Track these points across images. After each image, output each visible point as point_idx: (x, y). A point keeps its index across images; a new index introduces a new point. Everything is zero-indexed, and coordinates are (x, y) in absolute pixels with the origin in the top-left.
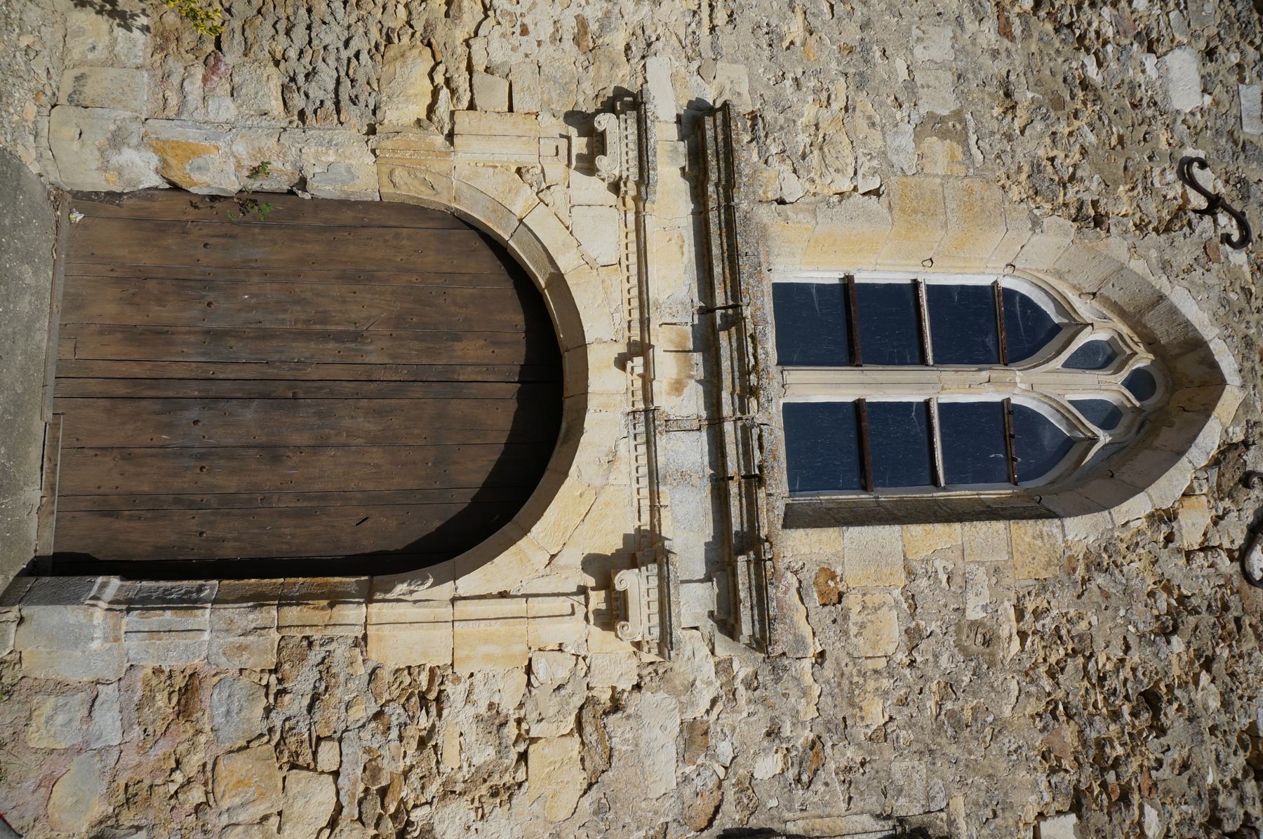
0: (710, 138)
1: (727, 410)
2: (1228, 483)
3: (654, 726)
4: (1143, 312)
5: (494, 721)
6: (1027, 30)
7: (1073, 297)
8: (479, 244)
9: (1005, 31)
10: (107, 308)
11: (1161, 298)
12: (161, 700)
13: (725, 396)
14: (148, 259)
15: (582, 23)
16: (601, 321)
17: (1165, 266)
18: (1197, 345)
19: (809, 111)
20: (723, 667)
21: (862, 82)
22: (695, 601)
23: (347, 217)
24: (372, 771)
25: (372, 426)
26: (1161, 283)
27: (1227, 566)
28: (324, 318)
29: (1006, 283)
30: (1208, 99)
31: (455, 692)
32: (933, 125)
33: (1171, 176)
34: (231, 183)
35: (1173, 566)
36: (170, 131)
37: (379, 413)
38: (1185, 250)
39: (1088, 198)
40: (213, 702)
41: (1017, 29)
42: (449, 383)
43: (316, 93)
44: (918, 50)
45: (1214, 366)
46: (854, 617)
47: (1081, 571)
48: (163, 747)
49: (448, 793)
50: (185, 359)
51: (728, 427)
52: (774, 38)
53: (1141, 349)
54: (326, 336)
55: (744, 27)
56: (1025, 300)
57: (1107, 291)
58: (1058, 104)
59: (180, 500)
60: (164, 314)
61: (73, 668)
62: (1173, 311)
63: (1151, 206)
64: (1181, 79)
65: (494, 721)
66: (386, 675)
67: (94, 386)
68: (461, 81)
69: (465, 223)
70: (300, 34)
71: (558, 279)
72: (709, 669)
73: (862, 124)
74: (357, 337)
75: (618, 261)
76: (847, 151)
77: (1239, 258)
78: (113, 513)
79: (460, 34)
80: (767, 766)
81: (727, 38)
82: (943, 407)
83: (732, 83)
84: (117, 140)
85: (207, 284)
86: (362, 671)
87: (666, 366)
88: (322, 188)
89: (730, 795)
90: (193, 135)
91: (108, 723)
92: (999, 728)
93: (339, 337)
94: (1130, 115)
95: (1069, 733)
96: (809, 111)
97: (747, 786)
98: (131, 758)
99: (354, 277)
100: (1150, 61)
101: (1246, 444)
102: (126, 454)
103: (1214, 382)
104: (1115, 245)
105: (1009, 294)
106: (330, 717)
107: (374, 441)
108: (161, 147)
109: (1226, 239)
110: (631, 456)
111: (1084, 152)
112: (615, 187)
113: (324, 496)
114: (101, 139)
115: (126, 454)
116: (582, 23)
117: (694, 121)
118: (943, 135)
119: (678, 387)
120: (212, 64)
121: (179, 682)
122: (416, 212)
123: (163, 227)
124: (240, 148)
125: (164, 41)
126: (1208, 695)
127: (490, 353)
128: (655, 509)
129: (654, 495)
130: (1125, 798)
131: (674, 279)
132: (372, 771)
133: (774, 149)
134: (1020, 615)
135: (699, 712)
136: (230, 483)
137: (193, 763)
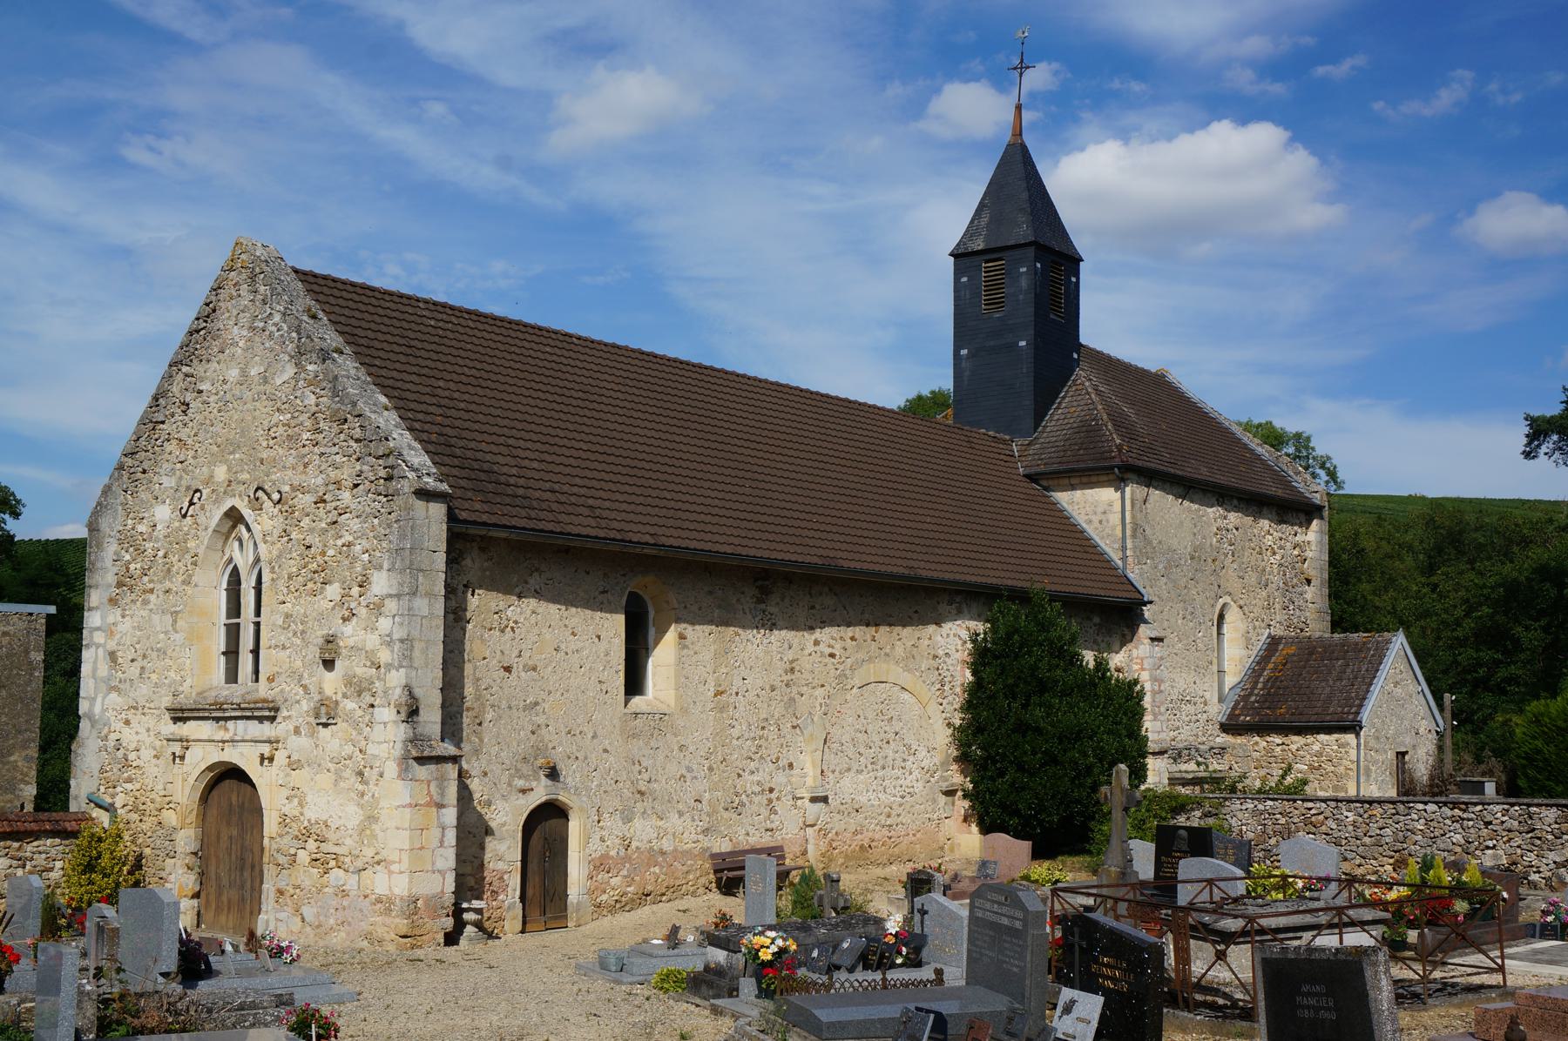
0: (180, 715)
9: (152, 591)
10: (223, 918)
16: (216, 756)
19: (172, 674)
29: (225, 585)
35: (276, 533)
38: (202, 519)
58: (169, 570)
64: (163, 513)
69: (205, 798)
71: (210, 768)
75: (208, 746)
87: (221, 735)
88: (193, 847)
91: (282, 915)
99: (218, 838)
100: (159, 527)
104: (201, 551)
117: (176, 720)
119: (227, 729)
122: (203, 817)
123: (207, 901)
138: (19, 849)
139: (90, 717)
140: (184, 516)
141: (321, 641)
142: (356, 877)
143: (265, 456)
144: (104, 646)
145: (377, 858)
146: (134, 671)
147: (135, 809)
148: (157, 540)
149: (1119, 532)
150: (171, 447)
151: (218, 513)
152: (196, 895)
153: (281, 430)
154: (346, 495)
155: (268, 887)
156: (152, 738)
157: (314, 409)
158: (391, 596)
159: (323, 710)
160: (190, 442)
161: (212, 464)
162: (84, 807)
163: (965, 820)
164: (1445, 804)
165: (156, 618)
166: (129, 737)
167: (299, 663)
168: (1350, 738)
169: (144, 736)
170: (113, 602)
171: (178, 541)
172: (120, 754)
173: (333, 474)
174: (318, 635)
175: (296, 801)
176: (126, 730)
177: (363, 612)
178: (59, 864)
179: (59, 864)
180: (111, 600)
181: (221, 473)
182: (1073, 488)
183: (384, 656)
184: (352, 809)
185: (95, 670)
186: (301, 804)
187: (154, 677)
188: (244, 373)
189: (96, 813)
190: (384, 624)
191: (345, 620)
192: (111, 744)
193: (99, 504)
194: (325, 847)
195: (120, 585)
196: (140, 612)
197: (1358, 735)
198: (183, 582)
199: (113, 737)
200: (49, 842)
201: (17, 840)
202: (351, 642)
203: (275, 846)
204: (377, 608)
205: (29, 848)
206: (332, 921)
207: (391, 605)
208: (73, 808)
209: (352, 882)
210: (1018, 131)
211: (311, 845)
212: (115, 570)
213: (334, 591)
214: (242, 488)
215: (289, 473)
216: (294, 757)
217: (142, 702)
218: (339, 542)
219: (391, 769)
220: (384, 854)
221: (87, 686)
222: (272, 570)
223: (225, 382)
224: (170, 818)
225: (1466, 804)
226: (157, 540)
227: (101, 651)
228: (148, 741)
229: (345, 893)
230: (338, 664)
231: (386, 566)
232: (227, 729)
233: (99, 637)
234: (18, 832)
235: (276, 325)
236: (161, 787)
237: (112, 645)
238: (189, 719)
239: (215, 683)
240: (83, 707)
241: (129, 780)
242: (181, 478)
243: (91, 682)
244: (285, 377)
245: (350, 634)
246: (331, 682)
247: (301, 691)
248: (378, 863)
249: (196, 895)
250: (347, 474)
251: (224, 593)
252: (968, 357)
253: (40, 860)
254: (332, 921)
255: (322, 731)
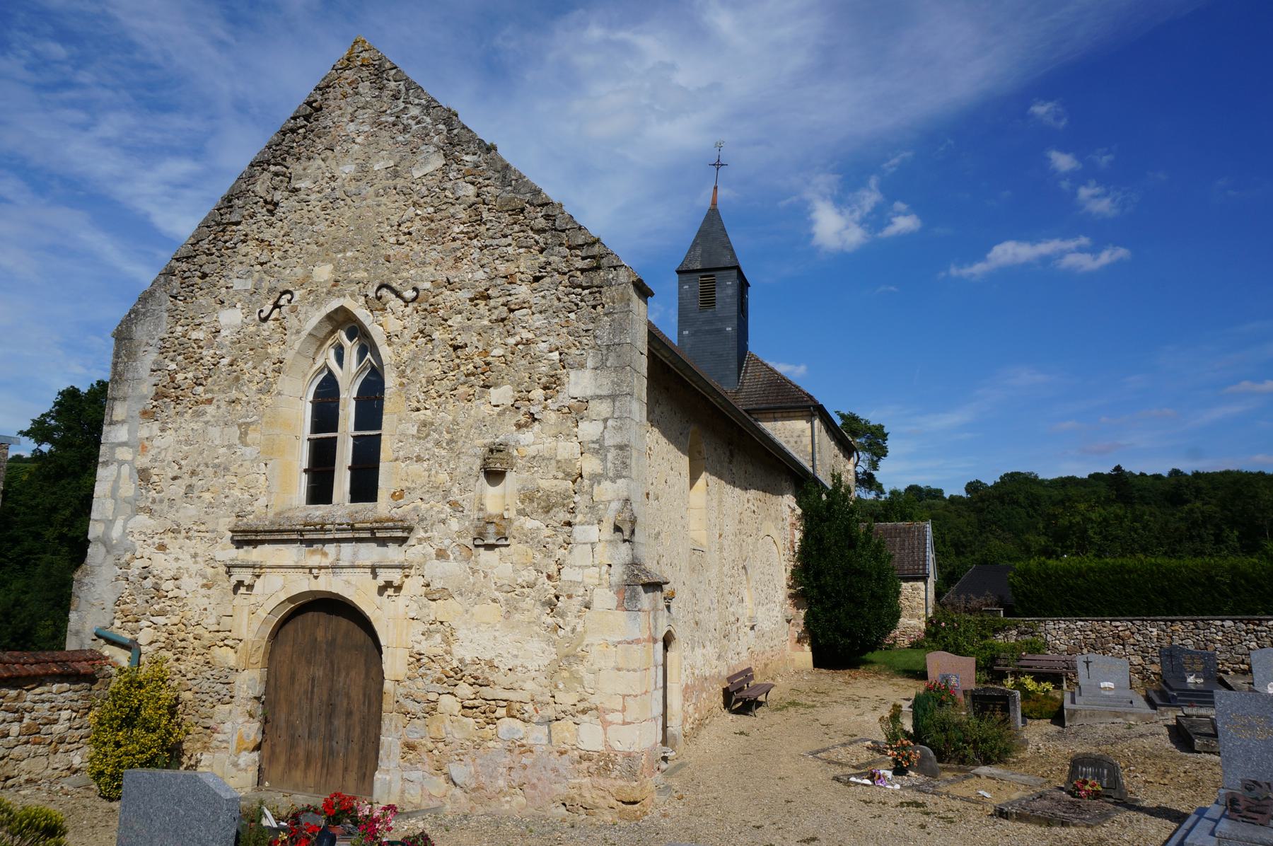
0: (246, 538)
1: (331, 536)
2: (380, 306)
3: (439, 571)
4: (318, 340)
5: (427, 634)
6: (212, 391)
7: (316, 367)
8: (283, 630)
9: (210, 401)
10: (298, 775)
11: (310, 334)
12: (410, 756)
13: (327, 537)
14: (283, 759)
15: (204, 586)
16: (303, 584)
17: (298, 332)
18: (329, 317)
19: (236, 492)
20: (420, 541)
21: (226, 469)
22: (393, 553)
23: (272, 682)
24: (439, 680)
25: (343, 674)
26: (304, 334)
27: (409, 310)
28: (306, 692)
29: (311, 397)
30: (239, 305)
31: (417, 648)
32: (243, 435)
33: (265, 325)
34: (256, 725)
35: (407, 335)
36: (233, 746)
37: (339, 671)
38: (292, 322)
39: (272, 367)
40: (413, 738)
41: (209, 396)
42: (332, 643)
43: (224, 692)
44: (216, 442)
45: (337, 310)
46: (408, 484)
47: (405, 380)
48: (424, 756)
49: (449, 653)
50: (317, 746)
51: (337, 536)
52: (210, 505)
53: (337, 335)
54: (312, 692)
55: (206, 518)
56: (318, 387)
57: (311, 354)
58: (237, 379)
59: (361, 750)
60: (301, 753)
61: (397, 787)
62: (315, 328)
63: (277, 336)
64: (231, 318)
65: (427, 634)
66: (409, 673)
67: (323, 781)
68: (222, 635)
69: (275, 635)
70: (204, 697)
71: (291, 600)
72: (419, 547)
73: (242, 469)
74: (313, 680)
75: (286, 575)
76: (250, 477)
77: (297, 295)
78: (365, 775)
79: (207, 635)
80: (454, 525)
81: (210, 526)
82: (357, 428)
83: (225, 524)
84: (235, 765)
85: (293, 737)
86: (408, 682)
87: (316, 560)
88: (258, 690)
89: (462, 541)
90: (235, 738)
91: (414, 775)
92: (455, 422)
93: (313, 687)
94: (243, 344)
95: (462, 389)
96: (236, 492)
97: (460, 534)
98: (426, 768)
99: (292, 679)
100: (223, 333)
101: (366, 296)
102: (346, 769)
103: (342, 309)
104: (289, 357)
105: (316, 395)
106: (419, 695)
107: (347, 674)
108: (239, 750)
109: (289, 301)
110: (347, 575)
111: (255, 368)
112: (258, 576)
113: (364, 695)
114: (234, 770)
115: (346, 769)
116: (204, 586)
117: (239, 544)
118: (246, 434)
119: (325, 554)
120: (215, 731)
121: (406, 749)
122: (271, 656)
123: (273, 752)
124: (240, 720)
125: (206, 748)
126: (456, 321)
127: (323, 627)
128: (364, 567)
129: (359, 567)
130: (488, 364)
131: (290, 554)
132: (439, 680)
133: (249, 508)
134: (418, 410)
135: (434, 552)
136: (358, 730)
137: (431, 746)
138: (16, 699)
139: (105, 541)
140: (265, 320)
141: (482, 451)
142: (545, 729)
143: (391, 253)
144: (131, 463)
145: (581, 706)
146: (178, 489)
147: (170, 646)
148: (220, 346)
149: (809, 449)
150: (251, 248)
151: (315, 317)
152: (258, 748)
153: (418, 224)
154: (522, 291)
155: (390, 740)
156: (201, 565)
157: (473, 199)
158: (600, 397)
159: (491, 529)
160: (277, 242)
161: (314, 260)
162: (88, 644)
163: (798, 641)
164: (1241, 621)
165: (214, 432)
166: (162, 564)
167: (443, 477)
168: (921, 584)
169: (187, 562)
170: (148, 415)
171: (249, 346)
172: (148, 583)
173: (503, 268)
174: (479, 444)
175: (438, 637)
176: (159, 558)
177: (552, 417)
178: (65, 714)
179: (65, 714)
180: (144, 413)
181: (324, 273)
182: (775, 420)
183: (590, 465)
184: (535, 646)
185: (114, 494)
186: (446, 641)
187: (207, 496)
188: (363, 169)
189: (108, 650)
190: (589, 430)
191: (519, 426)
192: (135, 570)
193: (134, 311)
194: (486, 692)
195: (158, 396)
196: (189, 424)
197: (926, 583)
198: (260, 391)
199: (138, 564)
200: (55, 687)
201: (15, 688)
202: (532, 451)
203: (401, 690)
204: (577, 411)
205: (29, 696)
206: (501, 783)
207: (604, 408)
208: (71, 644)
209: (536, 735)
210: (714, 203)
211: (464, 690)
212: (154, 380)
213: (503, 394)
214: (355, 288)
215: (431, 269)
216: (434, 586)
217: (186, 524)
218: (511, 341)
219: (605, 598)
220: (594, 700)
221: (102, 506)
222: (402, 374)
223: (333, 178)
224: (225, 656)
225: (1260, 620)
226: (220, 346)
227: (125, 470)
228: (194, 568)
229: (526, 750)
230: (510, 476)
231: (590, 363)
232: (325, 554)
233: (124, 454)
234: (18, 677)
235: (414, 118)
236: (212, 620)
237: (142, 461)
238: (262, 542)
239: (295, 503)
240: (95, 530)
241: (162, 613)
242: (261, 280)
243: (109, 504)
244: (429, 169)
245: (529, 441)
246: (495, 499)
247: (447, 508)
248: (584, 712)
249: (258, 748)
250: (527, 263)
251: (309, 406)
252: (688, 336)
253: (43, 710)
254: (501, 783)
255: (484, 555)
